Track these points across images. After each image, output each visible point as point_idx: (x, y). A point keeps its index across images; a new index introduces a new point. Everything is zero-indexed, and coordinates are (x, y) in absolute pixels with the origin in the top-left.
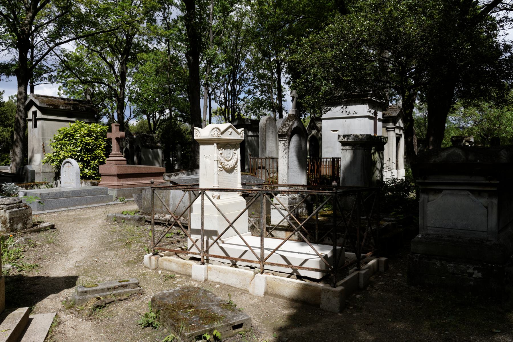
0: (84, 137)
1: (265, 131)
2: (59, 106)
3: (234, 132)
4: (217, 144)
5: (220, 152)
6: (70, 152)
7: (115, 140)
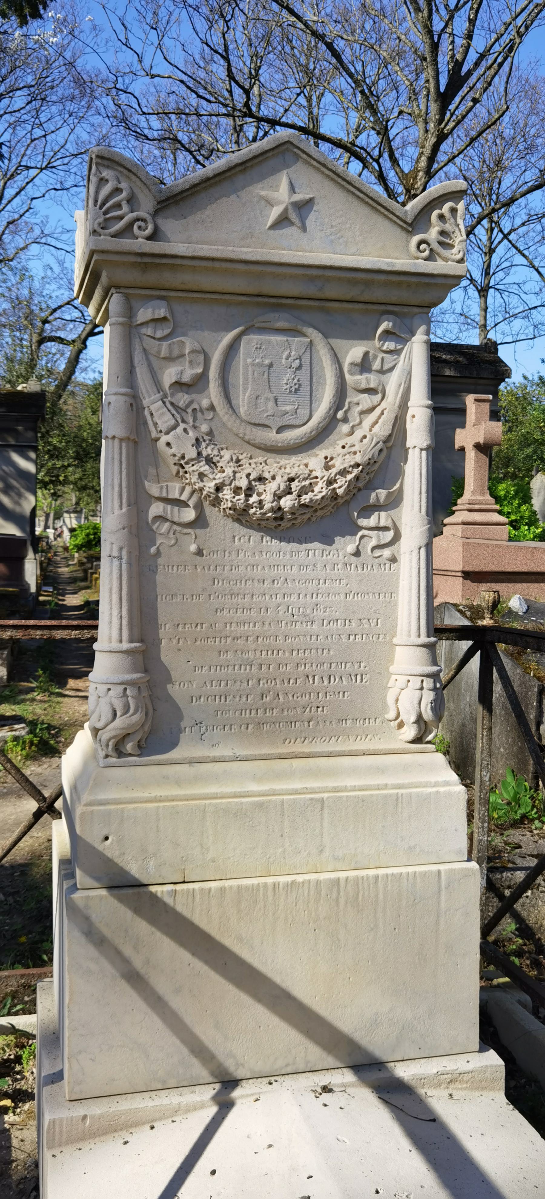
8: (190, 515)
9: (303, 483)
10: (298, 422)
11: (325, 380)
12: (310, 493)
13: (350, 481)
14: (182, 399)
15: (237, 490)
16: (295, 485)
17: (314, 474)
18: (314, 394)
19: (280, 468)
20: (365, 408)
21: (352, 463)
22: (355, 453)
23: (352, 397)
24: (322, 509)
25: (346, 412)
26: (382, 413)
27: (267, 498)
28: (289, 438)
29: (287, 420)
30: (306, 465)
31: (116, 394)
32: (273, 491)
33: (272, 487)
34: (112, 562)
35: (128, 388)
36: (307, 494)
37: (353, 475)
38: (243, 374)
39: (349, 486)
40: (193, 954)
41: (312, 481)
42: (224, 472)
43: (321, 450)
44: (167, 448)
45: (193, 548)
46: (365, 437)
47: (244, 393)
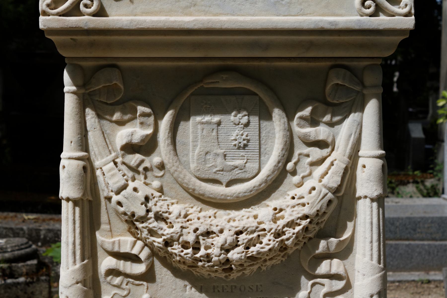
8: (140, 269)
9: (251, 236)
10: (247, 176)
11: (274, 134)
12: (258, 245)
13: (298, 233)
14: (134, 159)
15: (185, 245)
16: (243, 238)
17: (262, 226)
18: (263, 147)
19: (229, 222)
20: (314, 160)
21: (300, 215)
22: (304, 205)
23: (300, 149)
24: (271, 259)
25: (296, 164)
26: (332, 164)
27: (215, 251)
28: (238, 191)
29: (236, 174)
30: (256, 217)
32: (220, 245)
33: (218, 241)
35: (82, 150)
36: (255, 246)
37: (301, 227)
38: (193, 132)
39: (297, 237)
41: (261, 233)
42: (172, 227)
43: (271, 200)
44: (119, 207)
46: (314, 189)
47: (194, 150)
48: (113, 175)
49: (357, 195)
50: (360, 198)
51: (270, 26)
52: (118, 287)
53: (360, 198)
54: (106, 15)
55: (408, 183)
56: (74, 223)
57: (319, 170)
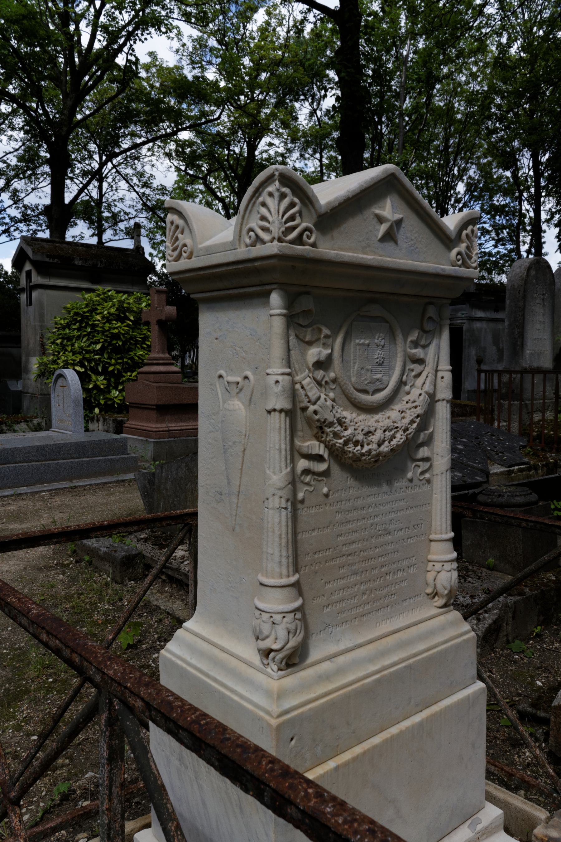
0: (109, 321)
1: (524, 297)
2: (74, 259)
3: (413, 228)
4: (290, 302)
5: (315, 353)
6: (80, 353)
7: (156, 327)
8: (322, 467)
10: (383, 386)
14: (320, 374)
17: (396, 425)
22: (416, 407)
29: (378, 385)
31: (283, 374)
32: (377, 441)
33: (375, 438)
34: (280, 512)
40: (224, 729)
43: (397, 404)
45: (325, 490)
47: (354, 367)
48: (311, 388)
49: (437, 399)
50: (439, 400)
51: (413, 268)
52: (308, 484)
53: (439, 400)
54: (316, 247)
55: (21, 422)
56: (286, 432)
57: (420, 381)
